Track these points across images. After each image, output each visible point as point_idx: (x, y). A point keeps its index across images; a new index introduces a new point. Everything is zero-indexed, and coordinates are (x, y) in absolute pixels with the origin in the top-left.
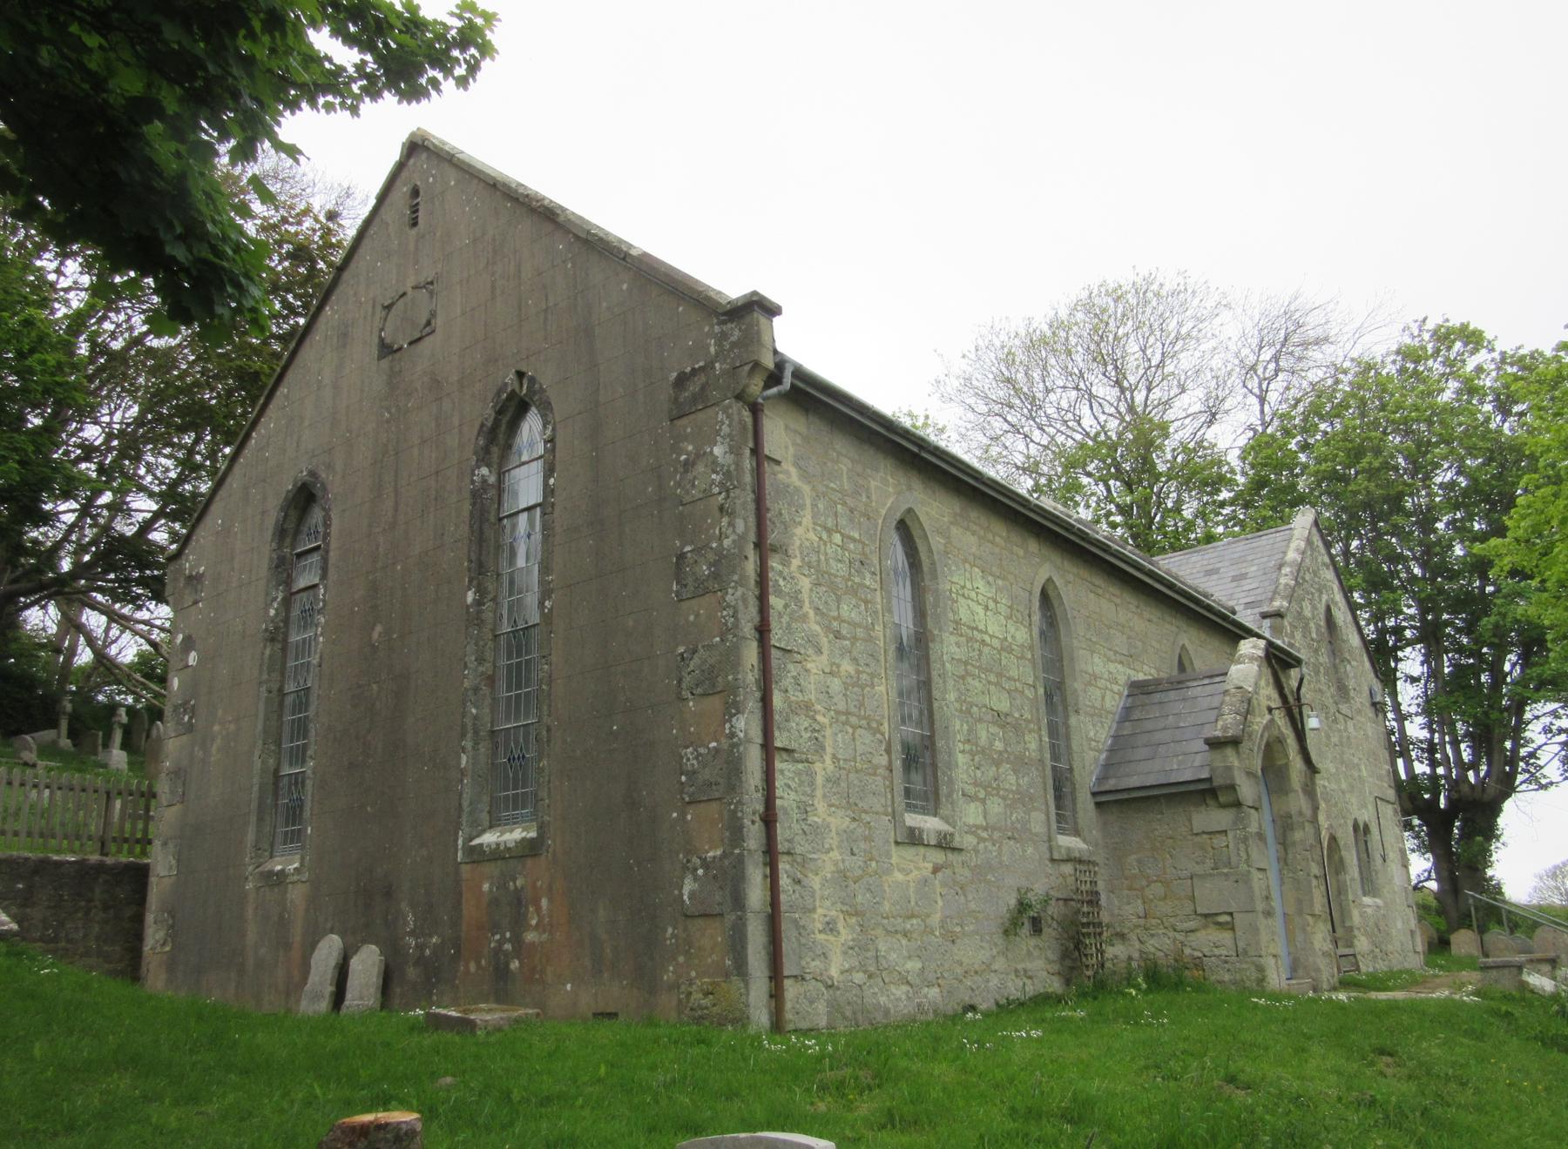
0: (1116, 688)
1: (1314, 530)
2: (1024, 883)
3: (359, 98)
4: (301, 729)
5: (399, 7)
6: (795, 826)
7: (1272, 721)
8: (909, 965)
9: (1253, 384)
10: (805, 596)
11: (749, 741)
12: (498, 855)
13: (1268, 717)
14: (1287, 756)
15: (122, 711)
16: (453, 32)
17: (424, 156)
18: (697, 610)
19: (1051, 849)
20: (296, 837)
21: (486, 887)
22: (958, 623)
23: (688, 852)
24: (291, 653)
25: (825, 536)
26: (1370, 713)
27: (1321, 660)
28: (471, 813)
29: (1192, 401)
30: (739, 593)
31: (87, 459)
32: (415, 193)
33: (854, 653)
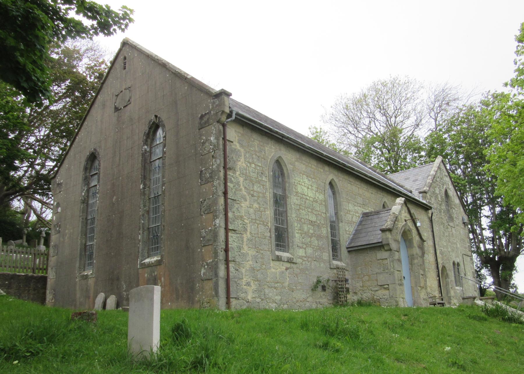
0: (357, 215)
1: (442, 164)
2: (320, 275)
3: (92, 35)
4: (92, 230)
5: (104, 7)
6: (236, 253)
7: (406, 224)
8: (276, 297)
9: (432, 114)
10: (241, 183)
11: (220, 226)
12: (149, 265)
13: (404, 223)
14: (412, 236)
15: (44, 233)
16: (121, 15)
17: (128, 46)
18: (206, 188)
19: (330, 265)
20: (91, 264)
21: (146, 275)
22: (297, 193)
23: (203, 261)
24: (89, 208)
25: (249, 165)
26: (462, 226)
27: (442, 208)
28: (142, 253)
29: (412, 120)
30: (217, 182)
31: (31, 148)
32: (125, 58)
33: (259, 201)
